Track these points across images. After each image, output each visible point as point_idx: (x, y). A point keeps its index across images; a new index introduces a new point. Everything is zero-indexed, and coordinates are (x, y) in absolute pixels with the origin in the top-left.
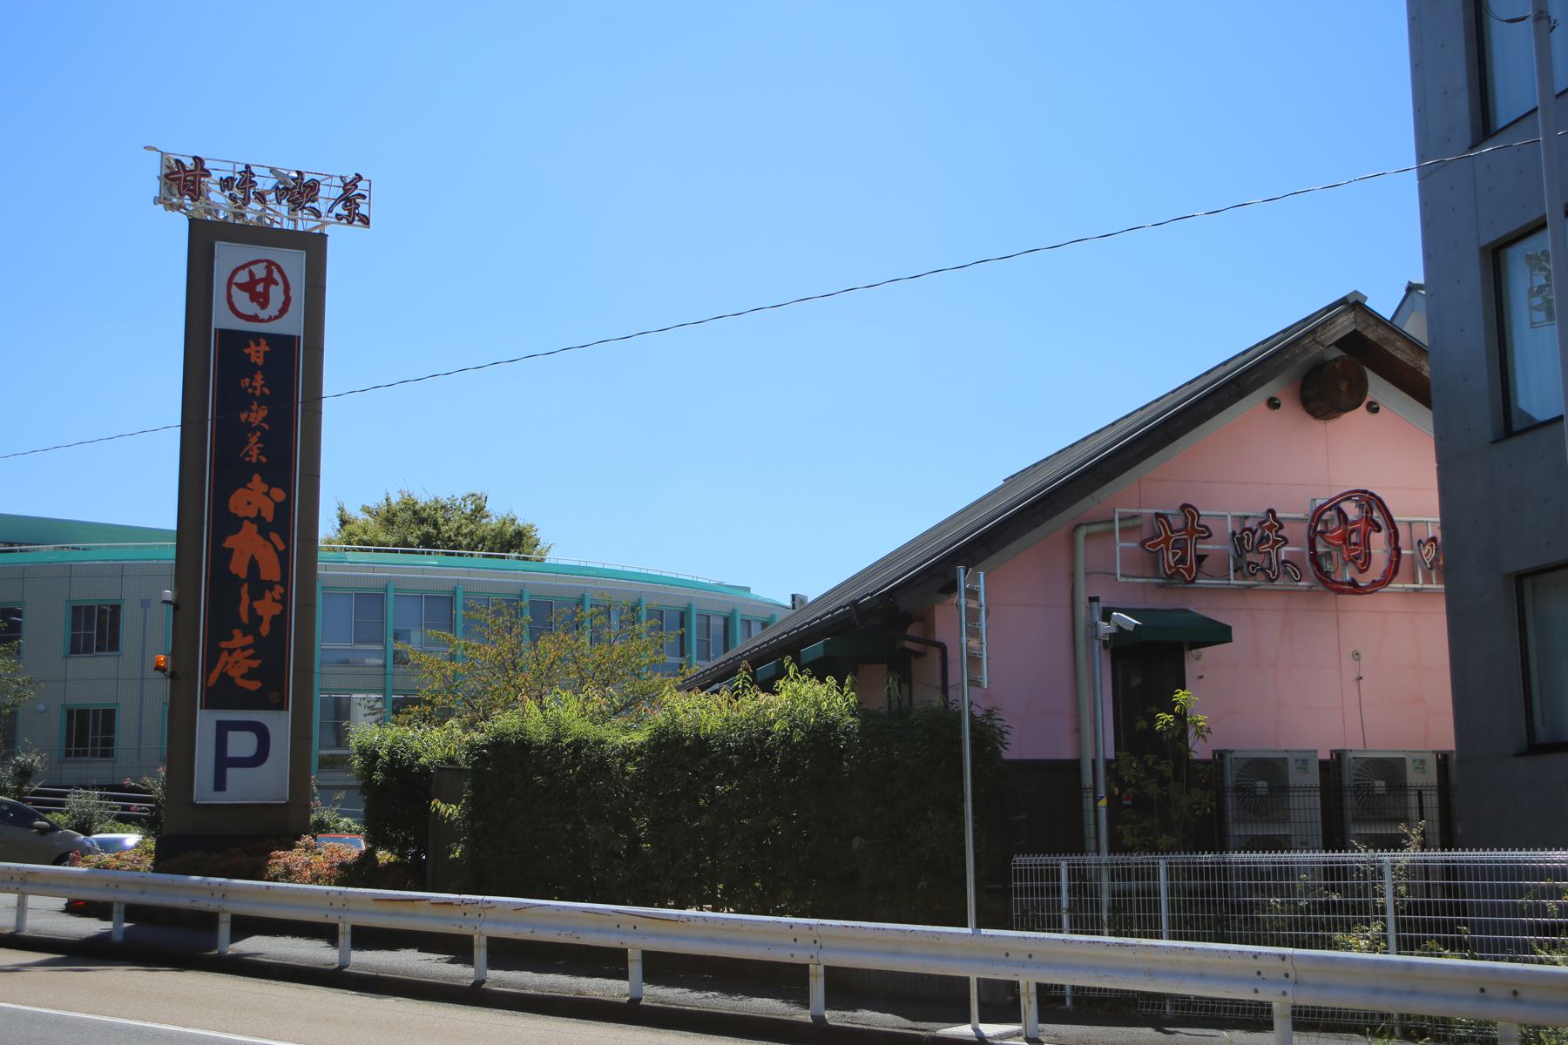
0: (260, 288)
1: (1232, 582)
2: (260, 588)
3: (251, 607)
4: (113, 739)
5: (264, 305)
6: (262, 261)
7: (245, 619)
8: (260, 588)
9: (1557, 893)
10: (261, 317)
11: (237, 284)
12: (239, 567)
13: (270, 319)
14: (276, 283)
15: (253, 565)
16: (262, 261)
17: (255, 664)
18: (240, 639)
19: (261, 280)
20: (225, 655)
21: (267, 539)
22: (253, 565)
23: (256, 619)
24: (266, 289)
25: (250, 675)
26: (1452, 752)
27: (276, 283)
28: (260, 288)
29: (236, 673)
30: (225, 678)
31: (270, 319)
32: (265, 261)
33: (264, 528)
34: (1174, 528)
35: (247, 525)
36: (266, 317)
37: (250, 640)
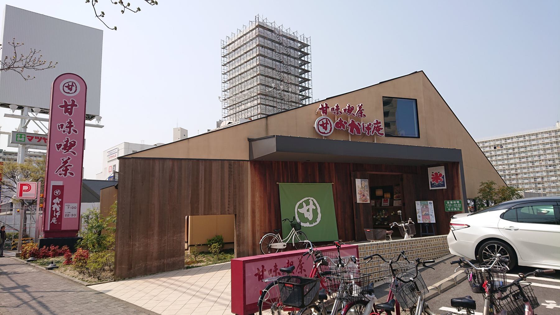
0: (325, 125)
1: (403, 225)
2: (57, 212)
3: (55, 214)
4: (297, 181)
5: (326, 130)
6: (325, 118)
7: (55, 216)
8: (57, 212)
9: (557, 187)
10: (326, 133)
11: (320, 125)
12: (54, 209)
13: (328, 133)
14: (329, 124)
15: (56, 209)
16: (325, 118)
17: (56, 221)
18: (54, 218)
19: (325, 123)
20: (52, 220)
21: (58, 205)
22: (56, 209)
23: (56, 216)
24: (326, 125)
25: (56, 222)
26: (262, 310)
27: (329, 124)
28: (325, 125)
29: (54, 222)
30: (53, 222)
31: (328, 133)
32: (326, 118)
33: (58, 204)
34: (247, 265)
35: (55, 204)
36: (327, 133)
37: (56, 218)
